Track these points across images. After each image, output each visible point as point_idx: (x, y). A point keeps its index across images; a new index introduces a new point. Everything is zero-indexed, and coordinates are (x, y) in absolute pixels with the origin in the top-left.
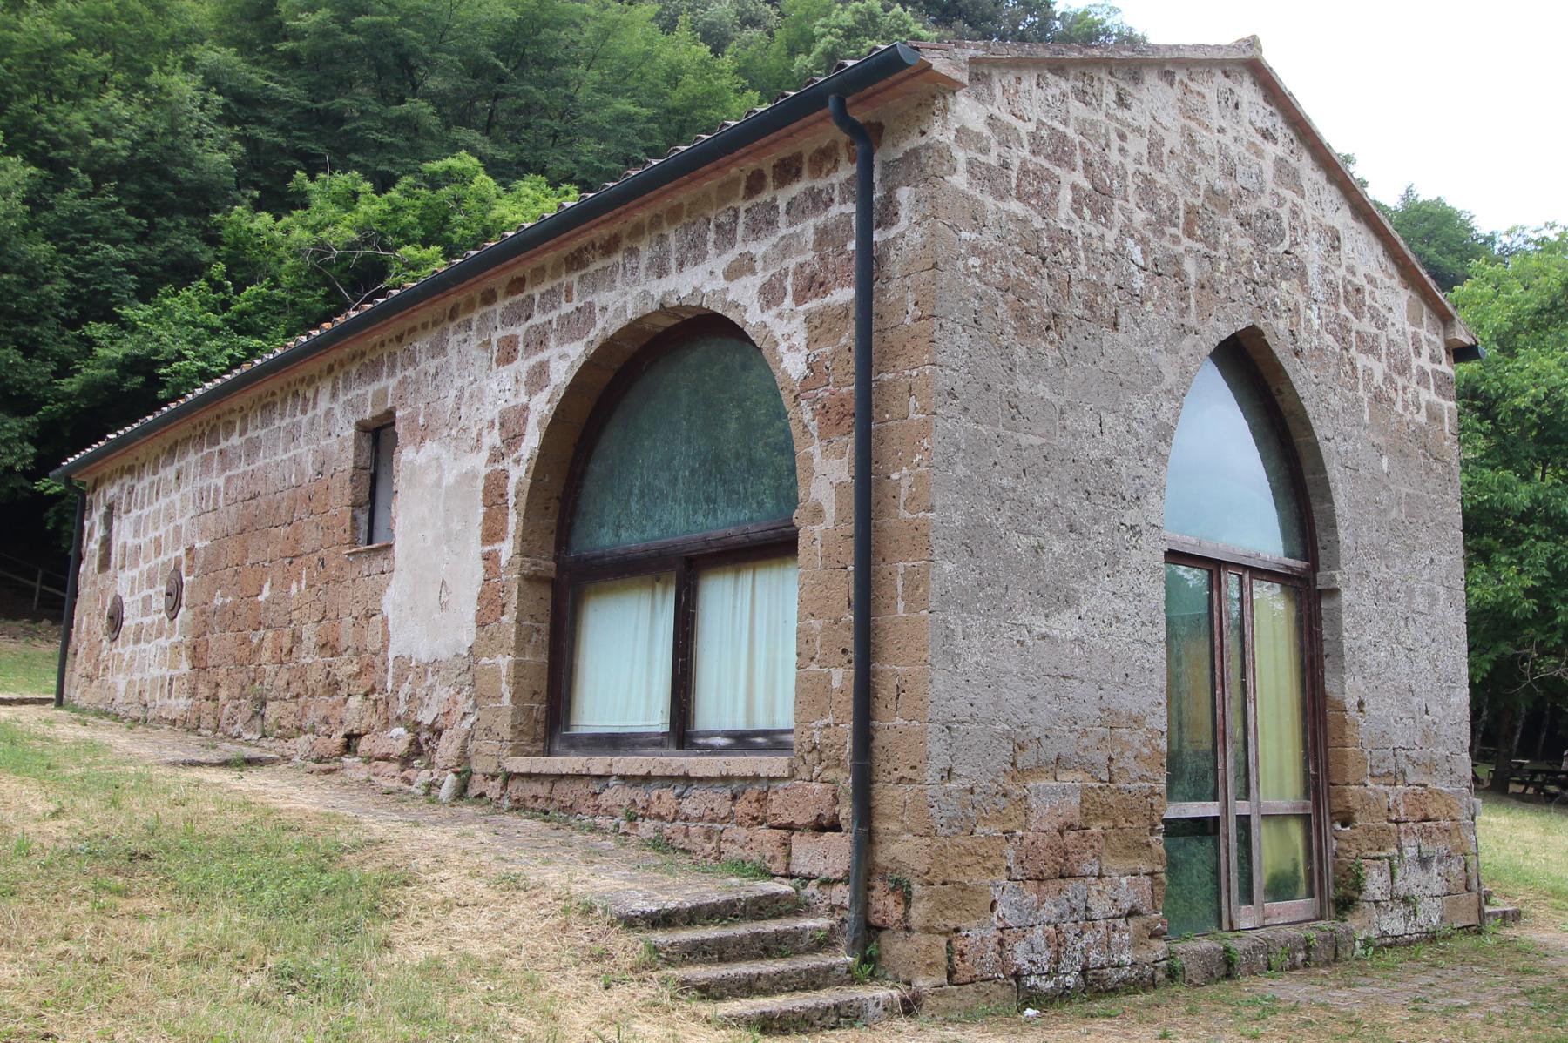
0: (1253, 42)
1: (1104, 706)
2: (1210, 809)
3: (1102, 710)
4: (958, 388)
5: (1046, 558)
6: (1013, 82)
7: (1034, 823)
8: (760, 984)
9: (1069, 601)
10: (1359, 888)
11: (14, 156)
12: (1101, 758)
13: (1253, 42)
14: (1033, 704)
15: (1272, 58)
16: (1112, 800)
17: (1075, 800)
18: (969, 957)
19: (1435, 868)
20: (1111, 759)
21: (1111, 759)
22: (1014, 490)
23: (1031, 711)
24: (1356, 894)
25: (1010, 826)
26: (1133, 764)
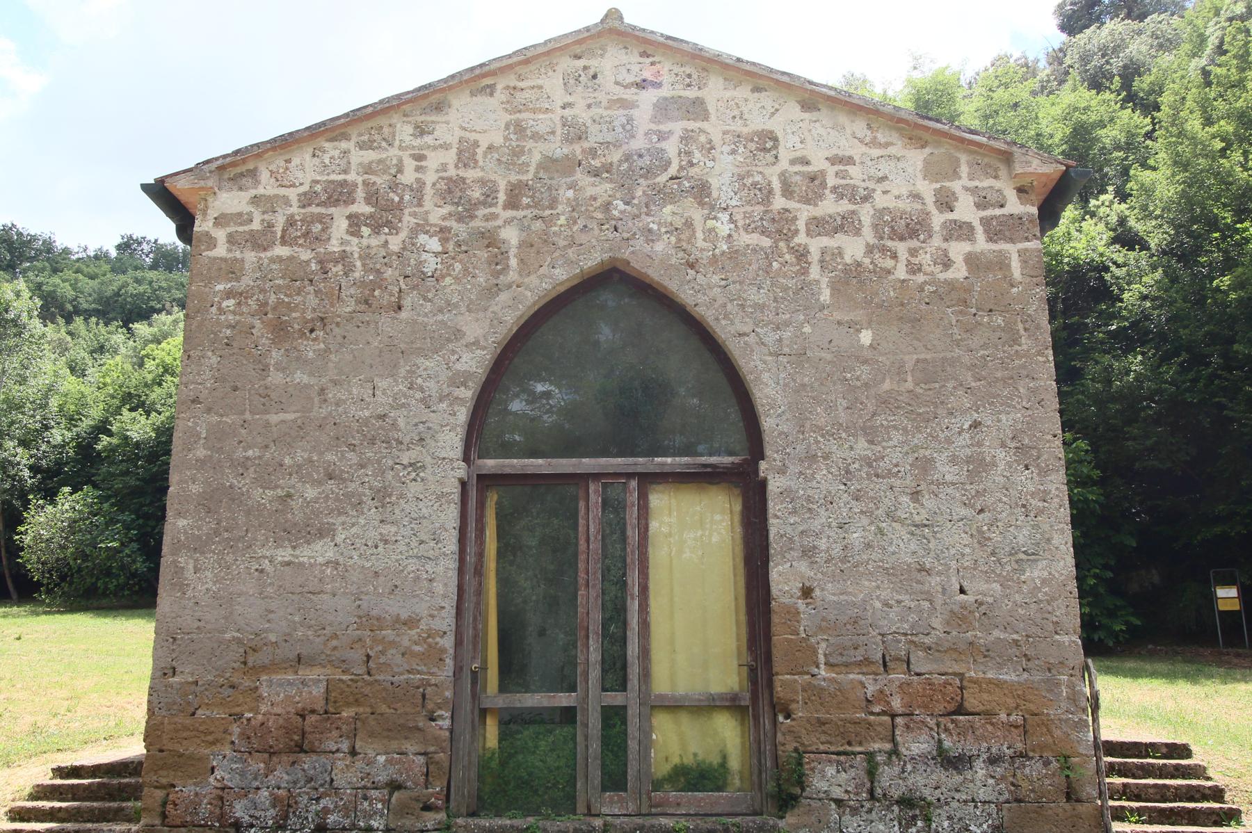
0: (613, 15)
1: (361, 614)
2: (564, 699)
3: (360, 617)
4: (202, 397)
5: (295, 504)
6: (282, 163)
7: (263, 709)
8: (60, 815)
9: (325, 532)
10: (802, 785)
11: (832, 295)
12: (357, 655)
13: (613, 15)
14: (271, 616)
15: (632, 18)
16: (367, 690)
17: (318, 691)
18: (181, 808)
19: (980, 770)
20: (368, 657)
21: (368, 657)
22: (260, 458)
23: (269, 621)
24: (798, 791)
25: (237, 710)
26: (399, 659)
